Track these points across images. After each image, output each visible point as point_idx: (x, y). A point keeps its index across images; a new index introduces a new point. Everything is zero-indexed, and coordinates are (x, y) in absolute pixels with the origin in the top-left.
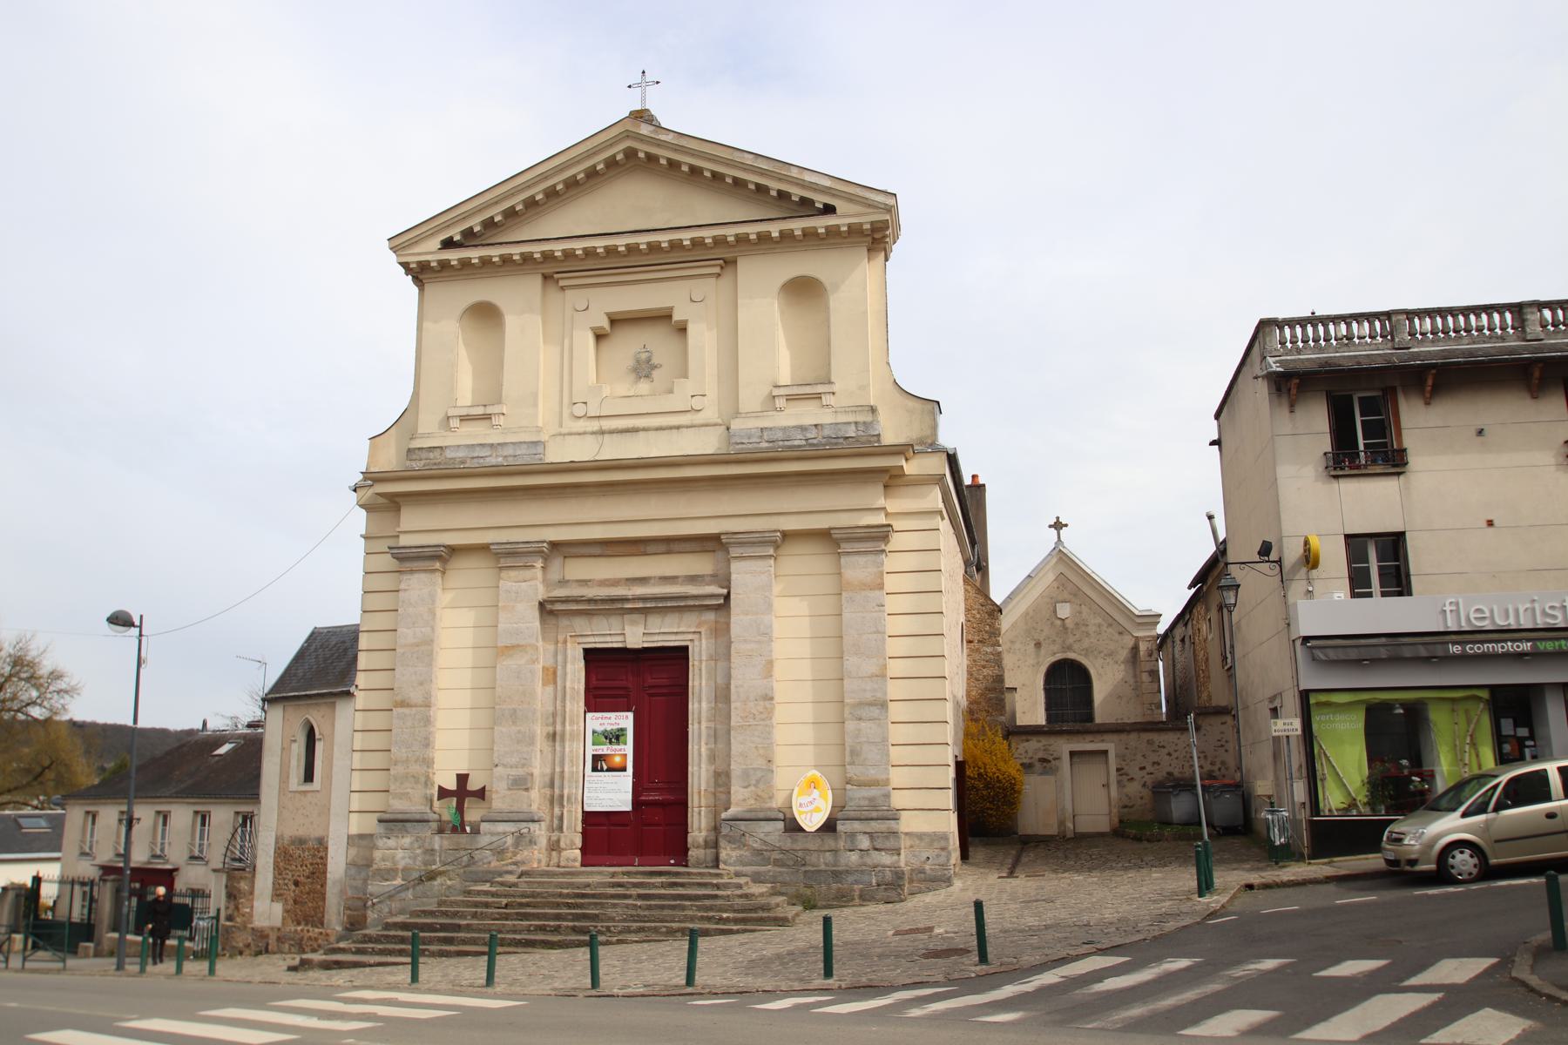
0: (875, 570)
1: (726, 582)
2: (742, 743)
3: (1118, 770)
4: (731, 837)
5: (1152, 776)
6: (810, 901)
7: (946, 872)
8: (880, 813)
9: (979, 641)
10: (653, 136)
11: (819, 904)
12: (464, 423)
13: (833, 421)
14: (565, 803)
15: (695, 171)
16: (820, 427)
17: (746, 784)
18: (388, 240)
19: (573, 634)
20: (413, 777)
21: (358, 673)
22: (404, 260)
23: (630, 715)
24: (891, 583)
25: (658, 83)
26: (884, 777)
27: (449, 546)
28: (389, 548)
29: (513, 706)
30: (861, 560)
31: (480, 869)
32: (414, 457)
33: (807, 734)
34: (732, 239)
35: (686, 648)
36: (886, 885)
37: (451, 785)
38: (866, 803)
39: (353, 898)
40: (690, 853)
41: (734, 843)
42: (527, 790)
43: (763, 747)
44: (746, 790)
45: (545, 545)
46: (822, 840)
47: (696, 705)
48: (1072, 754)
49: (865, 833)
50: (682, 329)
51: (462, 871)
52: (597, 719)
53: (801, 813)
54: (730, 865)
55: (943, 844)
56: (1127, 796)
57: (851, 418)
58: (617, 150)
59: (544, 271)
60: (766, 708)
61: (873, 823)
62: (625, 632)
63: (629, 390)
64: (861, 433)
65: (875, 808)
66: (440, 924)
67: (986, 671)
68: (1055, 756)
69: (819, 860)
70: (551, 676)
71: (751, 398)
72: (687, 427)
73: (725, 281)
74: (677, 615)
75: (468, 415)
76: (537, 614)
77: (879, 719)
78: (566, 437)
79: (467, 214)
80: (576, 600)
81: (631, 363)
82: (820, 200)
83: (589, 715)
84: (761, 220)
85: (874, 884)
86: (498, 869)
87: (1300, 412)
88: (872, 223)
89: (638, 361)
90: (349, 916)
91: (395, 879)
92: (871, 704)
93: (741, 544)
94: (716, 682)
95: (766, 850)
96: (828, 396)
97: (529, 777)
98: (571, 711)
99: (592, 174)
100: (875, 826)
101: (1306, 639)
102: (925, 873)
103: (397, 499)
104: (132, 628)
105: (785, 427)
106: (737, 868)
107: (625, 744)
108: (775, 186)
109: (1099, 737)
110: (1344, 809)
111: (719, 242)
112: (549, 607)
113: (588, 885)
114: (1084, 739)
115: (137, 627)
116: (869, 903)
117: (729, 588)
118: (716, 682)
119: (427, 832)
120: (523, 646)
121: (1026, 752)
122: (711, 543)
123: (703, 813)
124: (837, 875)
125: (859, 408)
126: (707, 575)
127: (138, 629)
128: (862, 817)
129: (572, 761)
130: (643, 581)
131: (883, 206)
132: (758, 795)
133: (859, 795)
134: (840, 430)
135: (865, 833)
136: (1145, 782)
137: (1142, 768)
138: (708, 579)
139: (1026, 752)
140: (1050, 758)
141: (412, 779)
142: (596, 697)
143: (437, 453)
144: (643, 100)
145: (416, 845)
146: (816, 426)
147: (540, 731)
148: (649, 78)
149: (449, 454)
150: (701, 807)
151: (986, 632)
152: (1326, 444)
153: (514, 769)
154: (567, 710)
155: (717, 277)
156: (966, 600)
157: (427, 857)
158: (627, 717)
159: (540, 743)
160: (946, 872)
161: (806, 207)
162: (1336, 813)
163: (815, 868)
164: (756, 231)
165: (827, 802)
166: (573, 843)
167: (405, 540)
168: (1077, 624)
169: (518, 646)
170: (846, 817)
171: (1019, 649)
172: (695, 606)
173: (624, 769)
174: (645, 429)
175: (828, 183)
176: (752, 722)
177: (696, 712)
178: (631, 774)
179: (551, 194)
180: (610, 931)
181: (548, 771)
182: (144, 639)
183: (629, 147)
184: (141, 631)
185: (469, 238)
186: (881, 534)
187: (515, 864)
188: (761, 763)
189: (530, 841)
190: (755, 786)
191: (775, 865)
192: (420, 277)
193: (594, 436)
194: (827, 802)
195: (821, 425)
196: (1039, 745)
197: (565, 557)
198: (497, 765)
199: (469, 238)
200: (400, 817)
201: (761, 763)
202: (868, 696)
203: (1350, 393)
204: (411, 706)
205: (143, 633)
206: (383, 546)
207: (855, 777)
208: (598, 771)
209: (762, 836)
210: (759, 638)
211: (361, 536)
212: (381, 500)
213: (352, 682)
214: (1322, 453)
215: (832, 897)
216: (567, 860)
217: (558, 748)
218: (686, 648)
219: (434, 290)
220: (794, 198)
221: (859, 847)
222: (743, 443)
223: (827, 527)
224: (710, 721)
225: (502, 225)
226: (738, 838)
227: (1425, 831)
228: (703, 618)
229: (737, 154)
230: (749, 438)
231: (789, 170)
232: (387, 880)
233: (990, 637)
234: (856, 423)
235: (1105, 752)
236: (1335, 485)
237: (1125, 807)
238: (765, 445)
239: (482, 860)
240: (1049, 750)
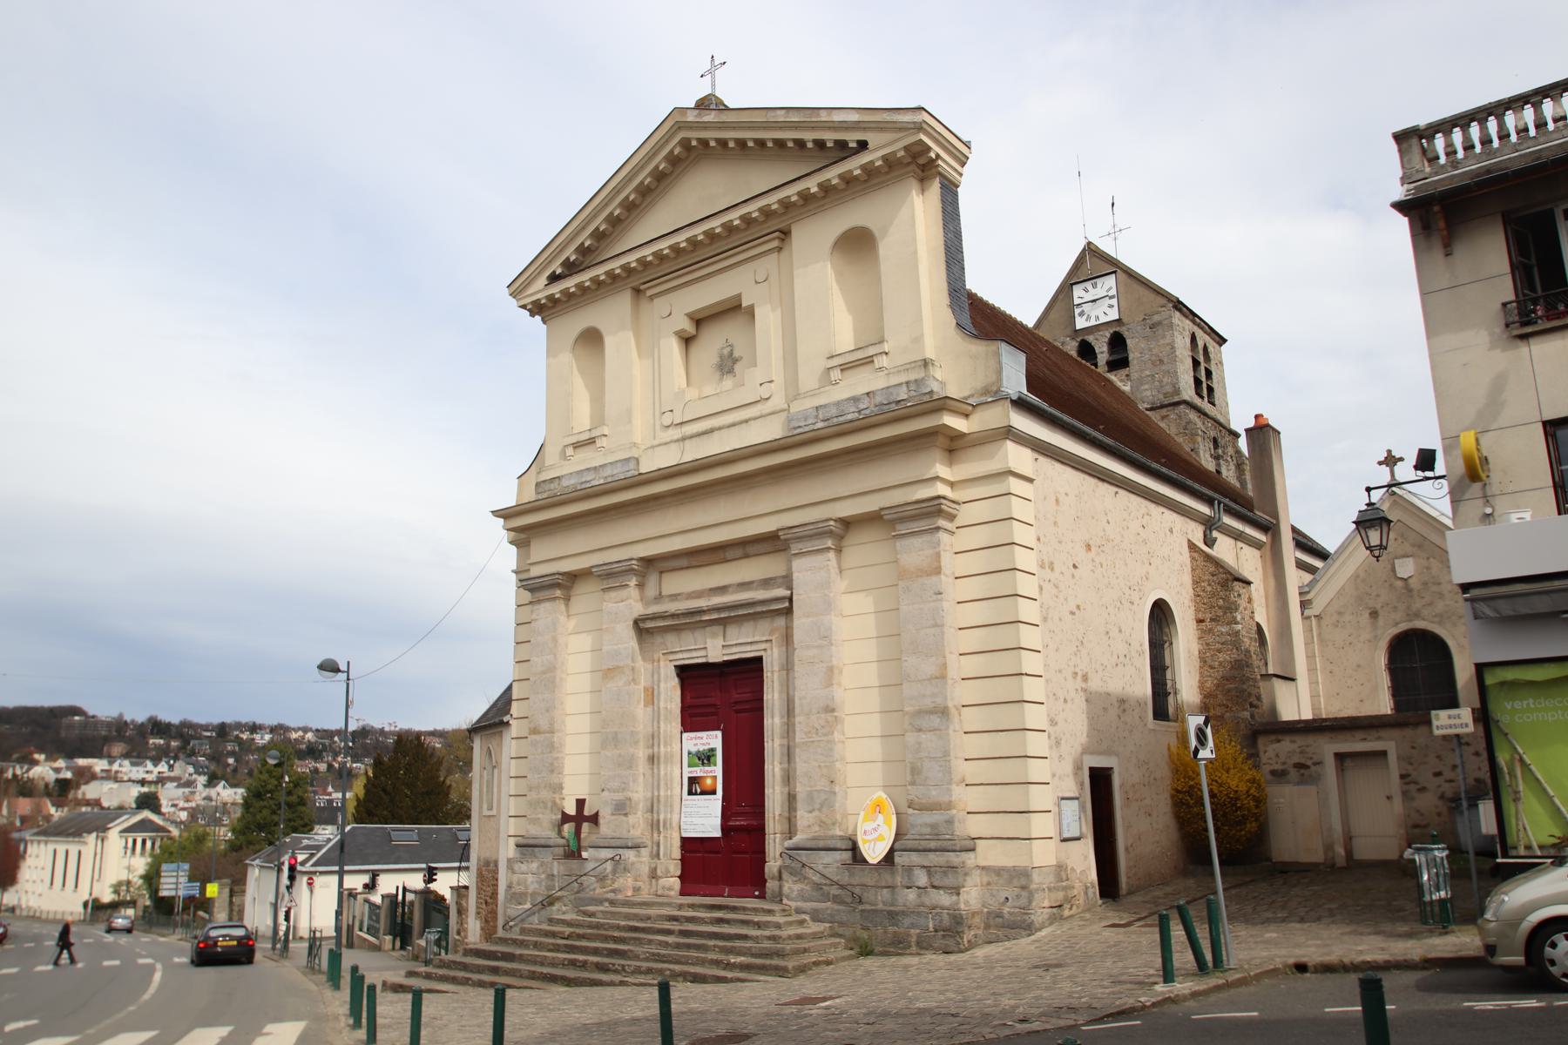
1: (787, 581)
2: (805, 762)
3: (1402, 777)
4: (792, 868)
5: (1453, 784)
6: (866, 947)
7: (1026, 917)
8: (940, 843)
9: (1212, 620)
10: (698, 120)
11: (878, 949)
12: (577, 450)
14: (661, 830)
16: (871, 395)
17: (811, 808)
18: (508, 287)
19: (665, 651)
20: (543, 802)
21: (513, 702)
22: (522, 303)
23: (719, 734)
26: (945, 799)
27: (565, 573)
30: (916, 542)
31: (588, 895)
33: (875, 749)
34: (902, 153)
35: (759, 660)
36: (944, 931)
37: (571, 810)
38: (928, 830)
40: (767, 884)
41: (795, 876)
42: (626, 815)
43: (826, 766)
44: (810, 815)
45: (634, 562)
46: (879, 874)
47: (770, 721)
48: (1340, 757)
51: (573, 897)
52: (691, 739)
53: (865, 841)
55: (1023, 881)
56: (1418, 811)
57: (903, 378)
59: (633, 284)
60: (827, 722)
61: (932, 856)
62: (707, 646)
63: (716, 389)
64: (913, 393)
65: (936, 836)
66: (502, 953)
67: (1222, 657)
68: (1316, 759)
69: (877, 899)
70: (651, 696)
71: (809, 377)
74: (752, 623)
75: (578, 442)
77: (940, 730)
79: (562, 246)
80: (662, 616)
81: (716, 360)
82: (852, 138)
83: (685, 735)
84: (799, 178)
85: (931, 929)
86: (600, 896)
87: (1461, 251)
88: (906, 148)
89: (721, 357)
91: (526, 904)
92: (932, 712)
93: (800, 539)
95: (825, 885)
96: (880, 357)
97: (628, 802)
98: (665, 731)
100: (934, 859)
101: (1466, 587)
102: (1002, 917)
104: (340, 674)
105: (839, 402)
106: (799, 903)
107: (715, 765)
108: (808, 136)
109: (1374, 733)
110: (1554, 846)
111: (767, 213)
113: (649, 918)
114: (1354, 736)
115: (343, 672)
116: (926, 952)
117: (790, 588)
119: (546, 856)
121: (1277, 756)
122: (772, 543)
123: (777, 840)
124: (893, 916)
125: (907, 367)
127: (346, 674)
128: (920, 848)
129: (666, 784)
130: (723, 589)
131: (912, 126)
132: (822, 822)
133: (921, 821)
135: (924, 867)
138: (780, 580)
139: (1277, 756)
140: (1309, 763)
141: (541, 805)
142: (691, 716)
144: (713, 85)
145: (541, 871)
146: (868, 394)
147: (642, 753)
149: (565, 483)
150: (775, 834)
151: (1220, 608)
152: (1505, 290)
154: (662, 731)
155: (779, 251)
156: (1193, 570)
157: (549, 883)
158: (716, 736)
159: (642, 766)
160: (1026, 917)
161: (843, 150)
162: (1539, 853)
163: (873, 908)
164: (796, 192)
165: (890, 830)
166: (668, 871)
168: (1425, 584)
169: (618, 667)
170: (903, 847)
171: (1350, 622)
172: (763, 612)
173: (714, 792)
174: (720, 428)
175: (854, 117)
176: (816, 738)
177: (770, 728)
178: (721, 798)
180: (624, 970)
181: (649, 795)
182: (351, 682)
184: (348, 676)
185: (571, 268)
186: (933, 510)
187: (613, 891)
188: (822, 784)
189: (625, 869)
190: (820, 810)
191: (835, 902)
193: (677, 444)
194: (890, 830)
195: (873, 392)
196: (1294, 747)
197: (661, 572)
198: (603, 790)
199: (571, 268)
200: (531, 842)
201: (822, 784)
202: (928, 703)
203: (1549, 206)
205: (350, 677)
208: (693, 794)
210: (820, 642)
211: (513, 571)
213: (507, 712)
214: (1499, 306)
215: (888, 942)
216: (663, 888)
217: (655, 771)
218: (759, 660)
221: (917, 884)
222: (800, 427)
224: (784, 738)
225: (597, 248)
226: (798, 870)
227: (1506, 899)
228: (775, 625)
229: (771, 114)
230: (805, 420)
231: (818, 115)
232: (520, 904)
233: (1225, 613)
234: (907, 383)
235: (1383, 754)
236: (1523, 350)
237: (1416, 826)
238: (820, 425)
239: (588, 886)
240: (1307, 753)
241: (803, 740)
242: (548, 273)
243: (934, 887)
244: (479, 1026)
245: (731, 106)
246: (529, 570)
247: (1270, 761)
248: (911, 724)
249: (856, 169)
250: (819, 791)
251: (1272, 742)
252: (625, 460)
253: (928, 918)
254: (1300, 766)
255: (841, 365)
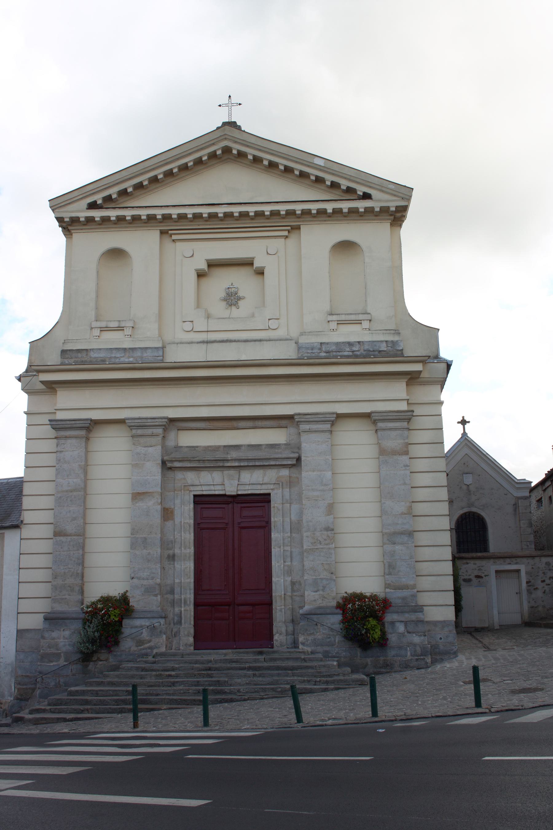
0: (402, 441)
3: (527, 582)
13: (370, 340)
15: (272, 165)
16: (362, 344)
17: (316, 589)
24: (415, 451)
25: (240, 104)
28: (50, 421)
29: (144, 536)
32: (67, 356)
35: (269, 494)
39: (22, 676)
44: (314, 594)
48: (497, 572)
49: (401, 621)
50: (260, 272)
54: (307, 645)
58: (217, 148)
60: (328, 536)
68: (486, 574)
72: (266, 340)
73: (291, 242)
76: (159, 469)
78: (179, 345)
90: (18, 689)
94: (290, 519)
99: (199, 162)
100: (407, 617)
103: (54, 386)
112: (169, 465)
118: (290, 519)
120: (151, 492)
126: (283, 444)
134: (375, 346)
135: (401, 621)
136: (545, 591)
137: (543, 581)
140: (483, 575)
143: (84, 354)
144: (230, 115)
146: (359, 342)
148: (234, 100)
153: (146, 581)
167: (60, 416)
176: (319, 546)
179: (169, 174)
183: (226, 146)
190: (323, 590)
192: (70, 228)
197: (178, 430)
198: (133, 578)
204: (68, 536)
206: (45, 419)
207: (392, 584)
209: (329, 625)
212: (43, 387)
219: (79, 237)
220: (97, 219)
223: (369, 411)
230: (312, 349)
234: (386, 341)
235: (518, 571)
238: (323, 354)
241: (309, 548)
242: (90, 200)
243: (409, 632)
244: (511, 680)
245: (243, 129)
246: (56, 413)
247: (463, 574)
248: (388, 540)
249: (362, 208)
250: (322, 579)
251: (464, 564)
252: (155, 348)
253: (406, 650)
254: (478, 577)
255: (337, 321)
